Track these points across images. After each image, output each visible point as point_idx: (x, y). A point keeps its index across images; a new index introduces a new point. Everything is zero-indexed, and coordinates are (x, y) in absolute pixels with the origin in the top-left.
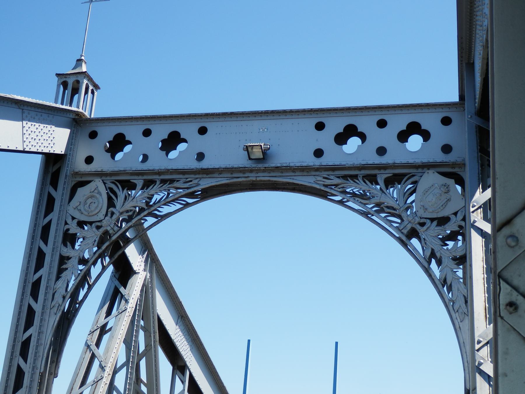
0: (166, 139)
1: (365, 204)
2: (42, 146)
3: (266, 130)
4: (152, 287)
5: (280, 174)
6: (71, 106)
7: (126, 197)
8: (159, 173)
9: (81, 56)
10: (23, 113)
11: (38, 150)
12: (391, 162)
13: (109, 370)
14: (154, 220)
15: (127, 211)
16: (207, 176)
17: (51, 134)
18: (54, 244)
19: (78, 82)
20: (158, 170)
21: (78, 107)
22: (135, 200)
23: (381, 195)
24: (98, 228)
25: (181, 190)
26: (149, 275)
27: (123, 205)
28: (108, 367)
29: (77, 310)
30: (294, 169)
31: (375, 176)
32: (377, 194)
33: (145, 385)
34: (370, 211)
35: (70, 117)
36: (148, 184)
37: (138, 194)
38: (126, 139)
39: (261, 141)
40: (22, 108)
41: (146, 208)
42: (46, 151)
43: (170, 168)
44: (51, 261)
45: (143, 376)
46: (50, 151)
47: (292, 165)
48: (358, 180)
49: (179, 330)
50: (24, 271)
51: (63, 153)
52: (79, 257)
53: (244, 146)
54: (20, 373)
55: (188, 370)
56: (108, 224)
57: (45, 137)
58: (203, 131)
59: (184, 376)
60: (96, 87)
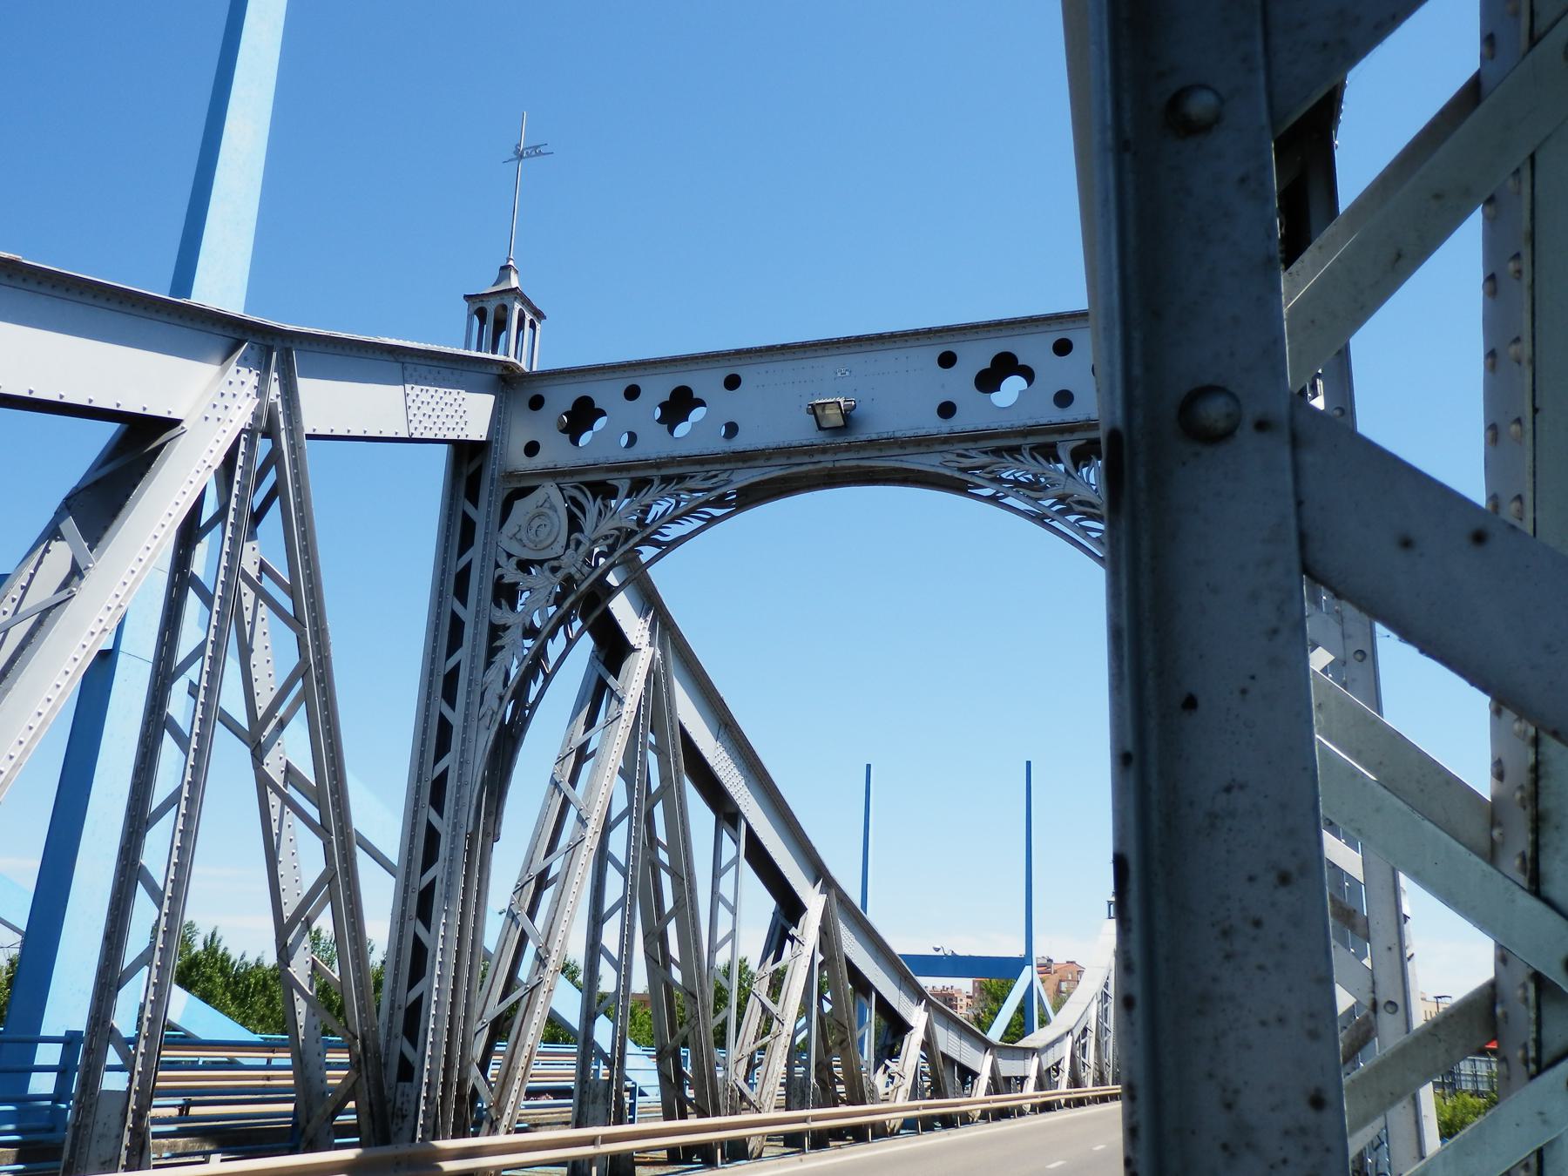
1: (1037, 499)
2: (444, 428)
4: (666, 674)
5: (877, 454)
6: (494, 351)
7: (600, 511)
8: (658, 464)
9: (509, 259)
10: (404, 369)
11: (436, 435)
12: (1081, 417)
13: (594, 825)
14: (656, 551)
15: (606, 537)
16: (745, 466)
17: (460, 405)
18: (478, 605)
19: (504, 308)
20: (655, 460)
21: (507, 354)
22: (617, 516)
23: (1064, 480)
24: (554, 570)
25: (700, 494)
26: (658, 652)
27: (597, 526)
28: (593, 819)
29: (526, 721)
30: (903, 442)
31: (1053, 446)
32: (1059, 480)
33: (665, 848)
34: (1046, 511)
35: (491, 372)
36: (638, 486)
37: (621, 504)
38: (695, 396)
39: (839, 394)
40: (401, 360)
41: (637, 529)
42: (452, 436)
43: (676, 454)
44: (475, 635)
45: (661, 834)
46: (459, 436)
47: (898, 434)
49: (722, 749)
50: (428, 654)
51: (484, 439)
52: (524, 624)
53: (809, 405)
54: (432, 836)
55: (743, 821)
56: (571, 562)
57: (449, 411)
58: (733, 382)
59: (736, 830)
60: (539, 315)
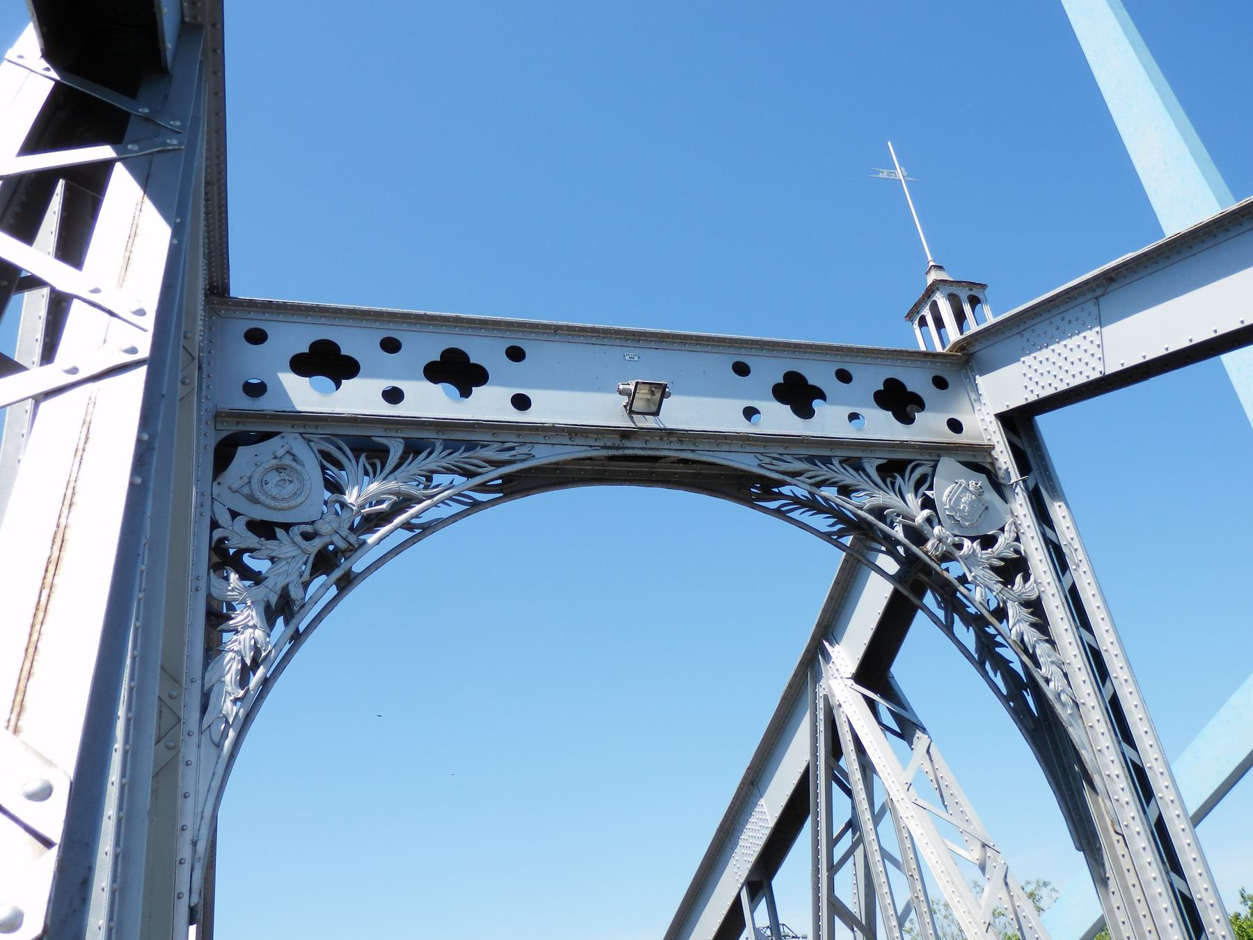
0: (469, 360)
3: (636, 358)
48: (832, 464)
